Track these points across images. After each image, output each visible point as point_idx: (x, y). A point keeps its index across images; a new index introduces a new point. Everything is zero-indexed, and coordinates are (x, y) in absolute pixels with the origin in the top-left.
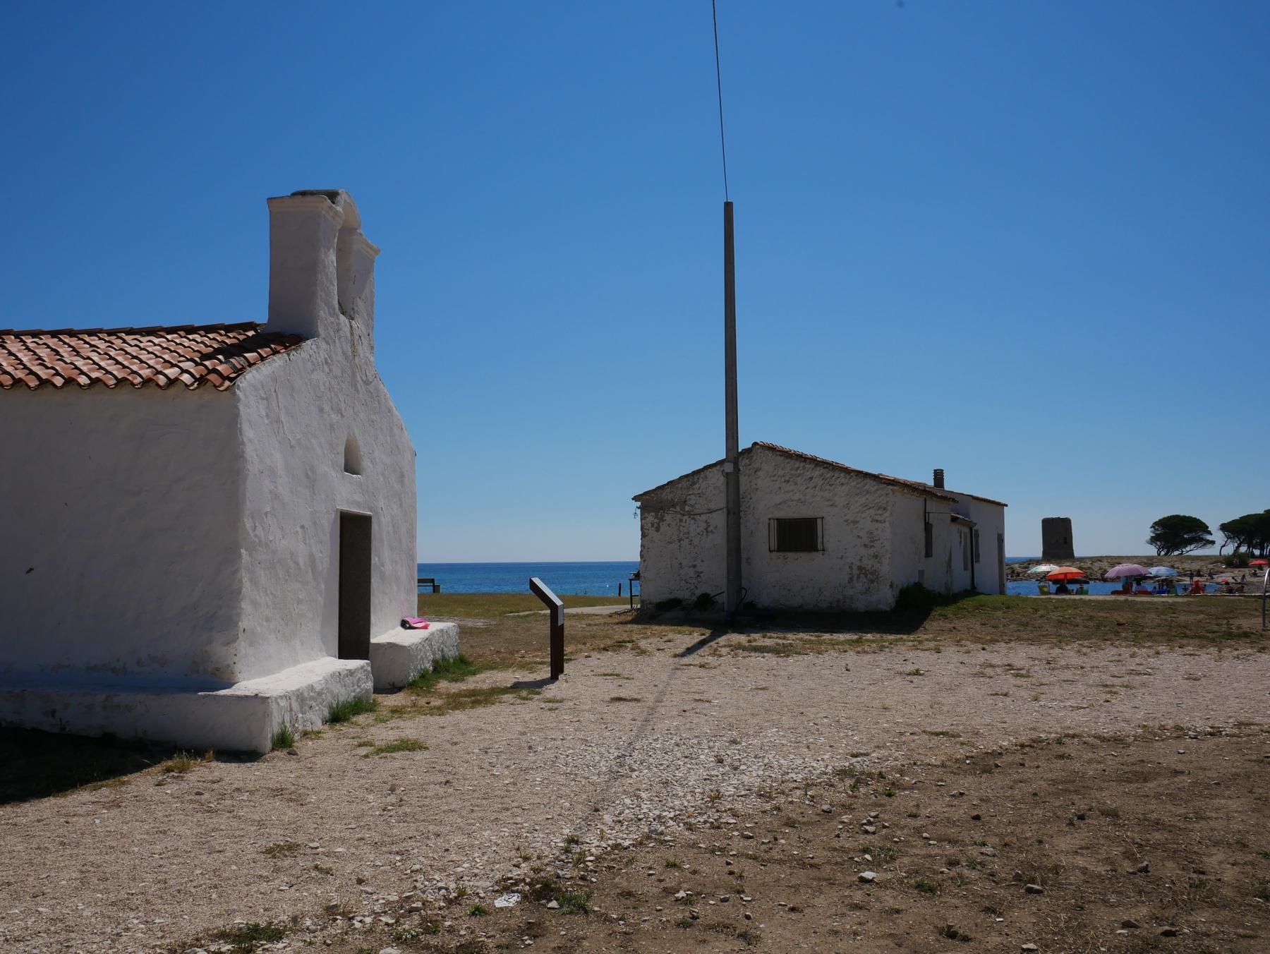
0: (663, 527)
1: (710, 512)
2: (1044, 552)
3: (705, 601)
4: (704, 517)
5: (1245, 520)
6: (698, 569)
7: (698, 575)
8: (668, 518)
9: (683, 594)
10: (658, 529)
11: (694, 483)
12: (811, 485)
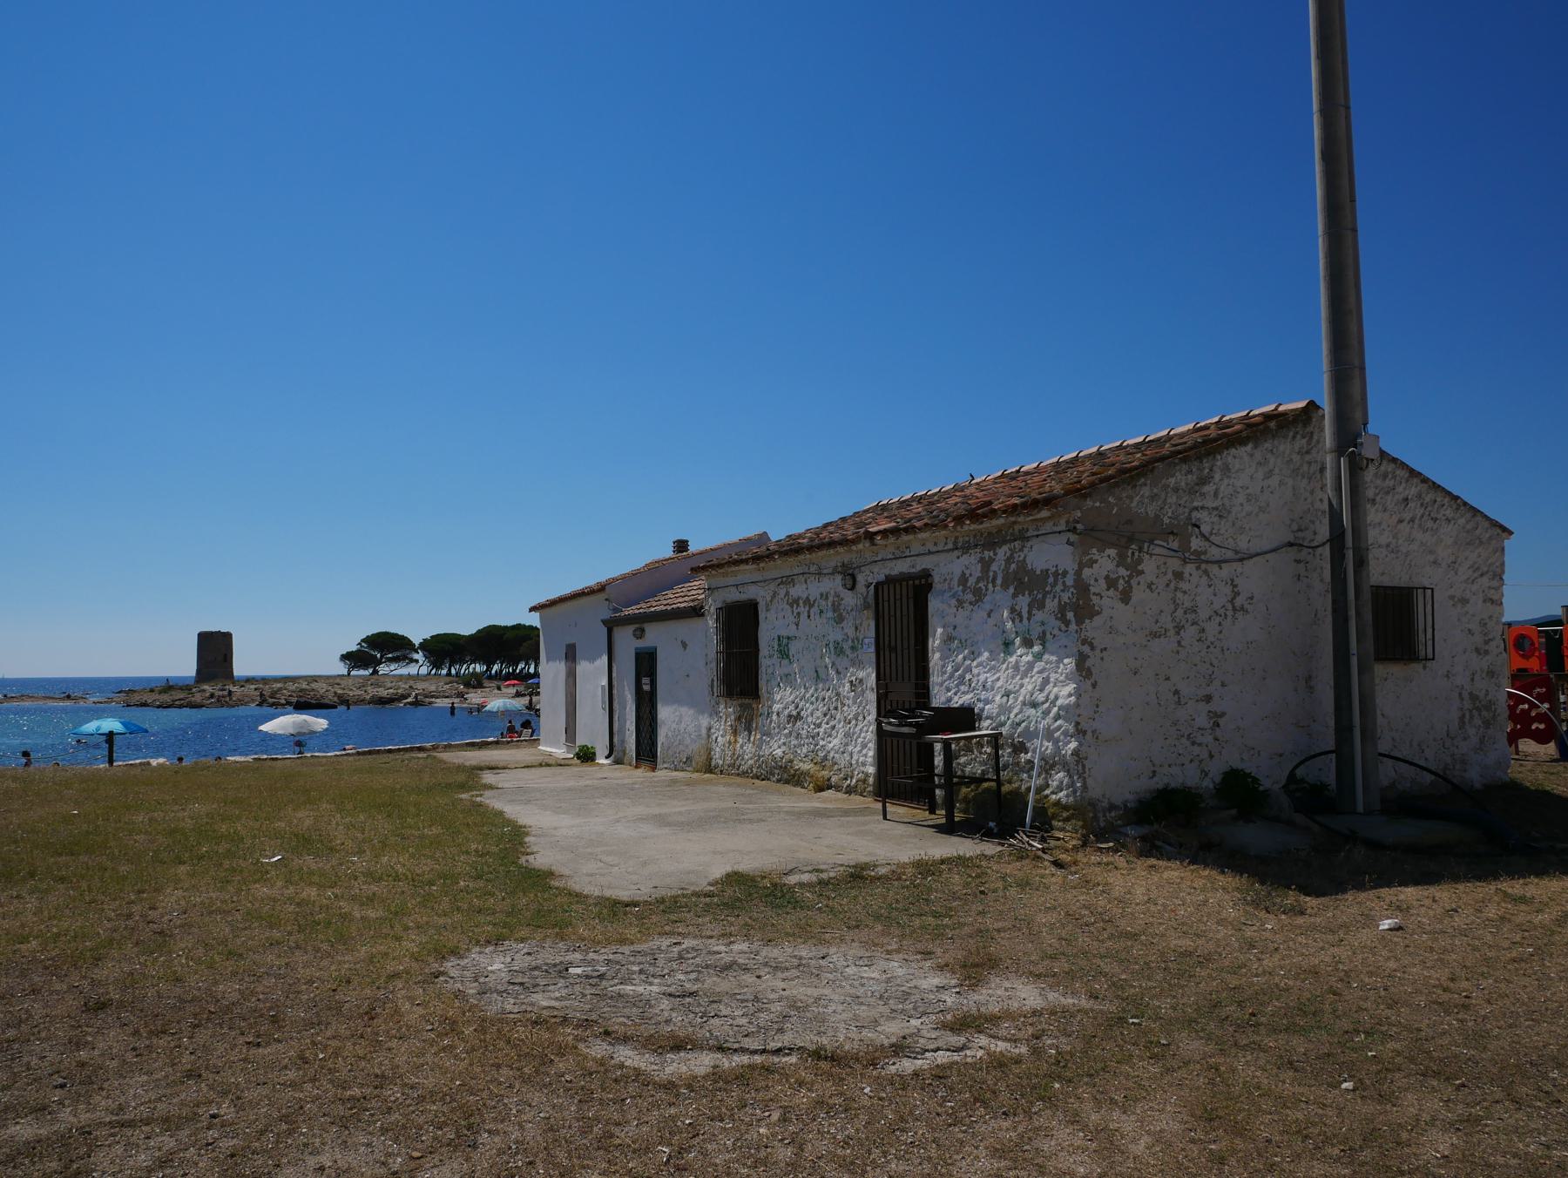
0: (1139, 594)
1: (1243, 558)
2: (198, 671)
3: (1239, 790)
4: (1227, 571)
5: (437, 638)
6: (1215, 706)
7: (1216, 718)
8: (1149, 566)
9: (1187, 776)
10: (1126, 597)
11: (1203, 481)
12: (1407, 516)
